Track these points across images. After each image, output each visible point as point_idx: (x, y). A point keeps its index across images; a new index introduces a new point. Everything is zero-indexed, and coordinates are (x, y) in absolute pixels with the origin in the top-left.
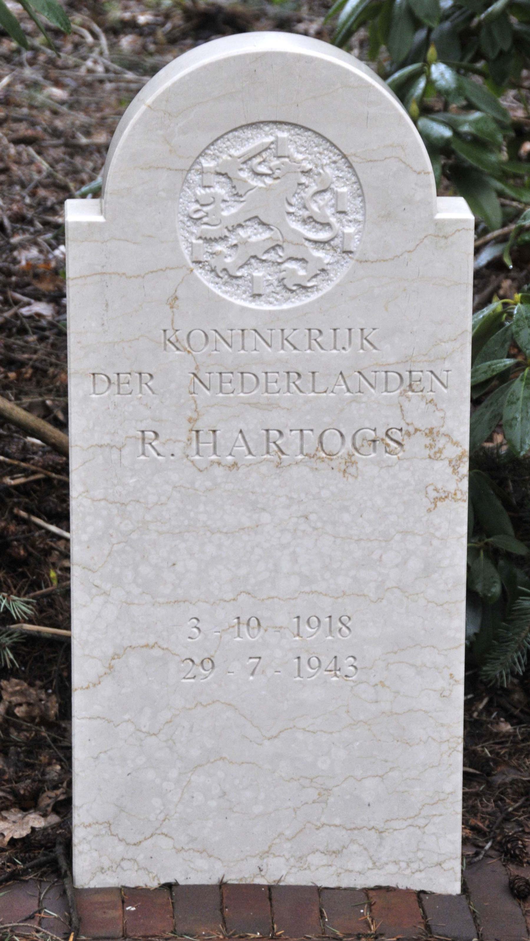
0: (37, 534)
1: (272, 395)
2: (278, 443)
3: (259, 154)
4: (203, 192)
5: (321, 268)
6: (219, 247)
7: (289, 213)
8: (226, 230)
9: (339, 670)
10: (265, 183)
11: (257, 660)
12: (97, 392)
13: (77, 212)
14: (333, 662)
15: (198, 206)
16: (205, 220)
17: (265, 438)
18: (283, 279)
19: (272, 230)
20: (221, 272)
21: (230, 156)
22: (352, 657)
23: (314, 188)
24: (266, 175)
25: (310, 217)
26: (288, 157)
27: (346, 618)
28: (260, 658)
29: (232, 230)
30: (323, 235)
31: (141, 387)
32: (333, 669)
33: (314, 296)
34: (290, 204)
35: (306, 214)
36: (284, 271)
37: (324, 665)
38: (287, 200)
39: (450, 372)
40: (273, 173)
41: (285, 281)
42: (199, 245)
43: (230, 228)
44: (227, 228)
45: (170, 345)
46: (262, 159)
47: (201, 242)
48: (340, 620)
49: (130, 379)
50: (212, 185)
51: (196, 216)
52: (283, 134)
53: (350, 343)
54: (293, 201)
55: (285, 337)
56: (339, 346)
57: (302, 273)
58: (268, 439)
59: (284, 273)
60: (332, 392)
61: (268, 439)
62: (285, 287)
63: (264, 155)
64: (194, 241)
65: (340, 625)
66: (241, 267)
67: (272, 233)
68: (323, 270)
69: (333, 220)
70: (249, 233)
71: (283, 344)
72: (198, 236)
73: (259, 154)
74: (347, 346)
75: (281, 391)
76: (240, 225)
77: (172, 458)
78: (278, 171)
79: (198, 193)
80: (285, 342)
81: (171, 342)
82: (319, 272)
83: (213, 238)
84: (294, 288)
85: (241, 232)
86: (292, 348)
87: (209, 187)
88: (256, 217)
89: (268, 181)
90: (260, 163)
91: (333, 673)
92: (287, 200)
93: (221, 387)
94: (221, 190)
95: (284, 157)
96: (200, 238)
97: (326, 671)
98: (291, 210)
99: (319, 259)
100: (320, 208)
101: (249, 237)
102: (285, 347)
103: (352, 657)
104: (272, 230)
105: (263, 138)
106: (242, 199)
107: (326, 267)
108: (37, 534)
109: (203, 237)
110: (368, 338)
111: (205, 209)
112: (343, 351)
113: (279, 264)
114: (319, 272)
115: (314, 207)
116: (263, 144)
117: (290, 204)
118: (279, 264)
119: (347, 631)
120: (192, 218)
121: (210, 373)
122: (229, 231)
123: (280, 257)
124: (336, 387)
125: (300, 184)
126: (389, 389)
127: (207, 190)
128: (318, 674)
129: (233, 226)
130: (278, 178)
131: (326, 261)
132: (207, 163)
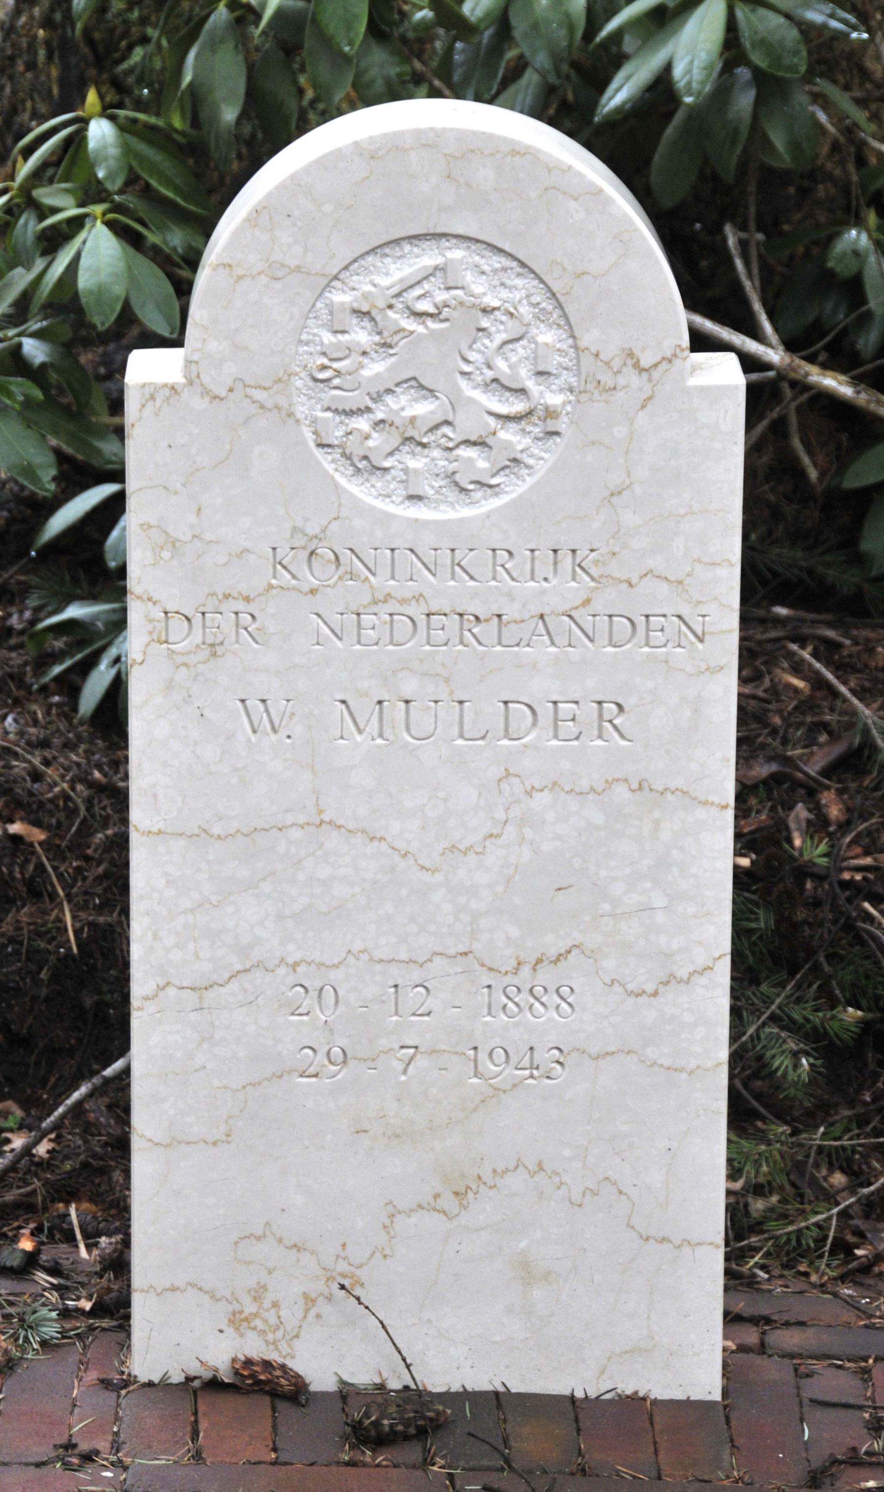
0: (115, 855)
1: (654, 650)
2: (616, 722)
3: (419, 282)
4: (333, 339)
5: (512, 456)
6: (362, 424)
7: (463, 373)
8: (367, 398)
9: (537, 1068)
10: (427, 327)
11: (412, 1051)
12: (651, 644)
13: (144, 367)
14: (528, 1055)
15: (325, 361)
16: (336, 382)
17: (595, 715)
18: (454, 473)
19: (437, 398)
20: (360, 461)
21: (375, 285)
22: (310, 1048)
23: (499, 338)
24: (431, 315)
25: (495, 380)
26: (463, 288)
27: (541, 989)
28: (416, 1047)
29: (377, 398)
30: (518, 406)
31: (237, 631)
32: (528, 1065)
33: (504, 499)
34: (466, 360)
35: (490, 374)
36: (456, 460)
37: (514, 1059)
38: (460, 352)
39: (707, 618)
40: (440, 313)
41: (457, 477)
42: (326, 420)
43: (375, 396)
44: (368, 394)
45: (284, 572)
46: (421, 292)
47: (329, 414)
48: (557, 991)
49: (446, 623)
50: (347, 329)
51: (321, 376)
52: (457, 254)
53: (555, 571)
54: (473, 356)
55: (456, 561)
56: (539, 575)
57: (482, 464)
58: (600, 716)
59: (455, 464)
60: (528, 645)
61: (600, 716)
62: (456, 484)
63: (426, 286)
64: (320, 414)
65: (505, 1000)
66: (391, 454)
67: (437, 403)
68: (515, 460)
69: (530, 384)
70: (403, 403)
71: (574, 571)
72: (326, 406)
73: (419, 282)
74: (550, 576)
75: (450, 643)
76: (389, 391)
77: (288, 741)
78: (446, 309)
79: (326, 341)
80: (457, 569)
81: (284, 567)
82: (508, 463)
83: (354, 409)
84: (471, 487)
85: (389, 399)
86: (467, 578)
87: (343, 332)
88: (414, 379)
89: (432, 325)
90: (419, 297)
91: (527, 1072)
92: (460, 352)
93: (359, 635)
94: (362, 336)
95: (457, 288)
96: (328, 409)
97: (516, 1069)
98: (467, 368)
99: (508, 445)
100: (510, 366)
101: (403, 409)
102: (577, 578)
103: (310, 1048)
104: (437, 398)
105: (428, 258)
106: (391, 351)
107: (518, 456)
108: (115, 855)
109: (333, 408)
110: (462, 563)
111: (335, 365)
112: (545, 584)
113: (450, 449)
114: (508, 463)
115: (501, 364)
116: (425, 268)
117: (466, 360)
118: (450, 449)
119: (516, 1009)
120: (316, 380)
121: (594, 616)
122: (372, 399)
123: (450, 439)
124: (534, 638)
125: (480, 330)
126: (396, 638)
127: (340, 337)
128: (507, 1072)
129: (378, 392)
130: (447, 320)
131: (520, 447)
132: (340, 297)
